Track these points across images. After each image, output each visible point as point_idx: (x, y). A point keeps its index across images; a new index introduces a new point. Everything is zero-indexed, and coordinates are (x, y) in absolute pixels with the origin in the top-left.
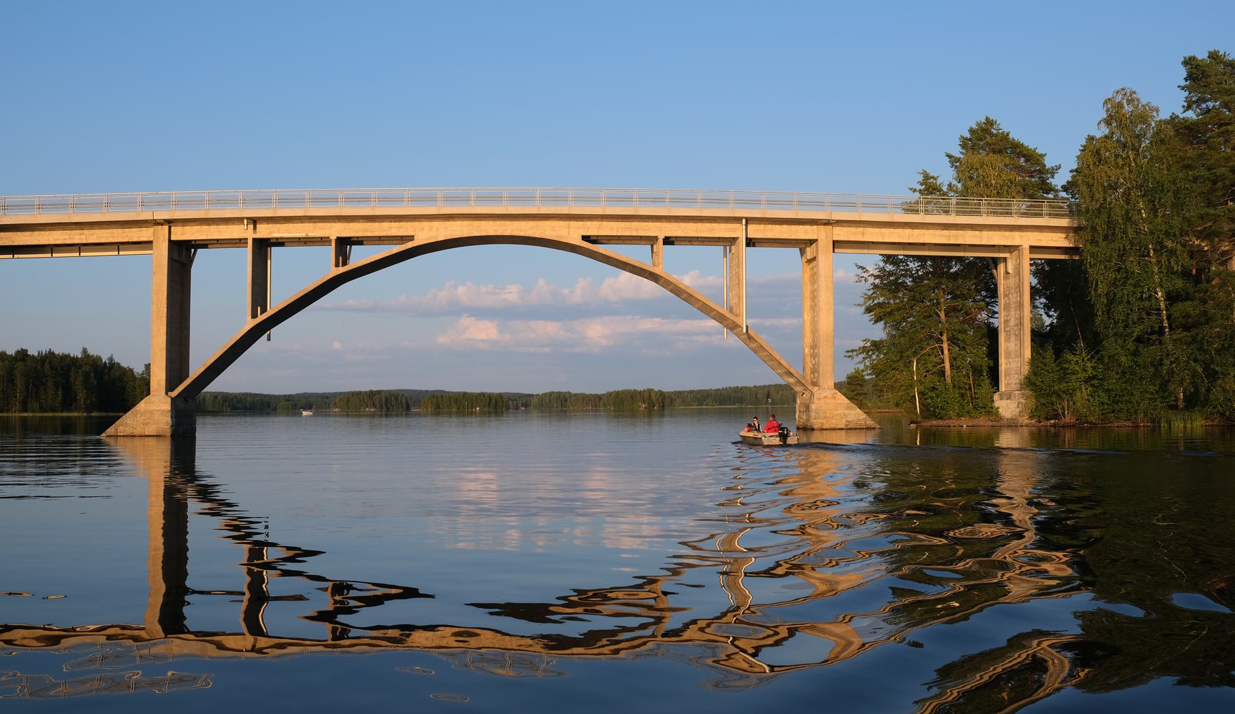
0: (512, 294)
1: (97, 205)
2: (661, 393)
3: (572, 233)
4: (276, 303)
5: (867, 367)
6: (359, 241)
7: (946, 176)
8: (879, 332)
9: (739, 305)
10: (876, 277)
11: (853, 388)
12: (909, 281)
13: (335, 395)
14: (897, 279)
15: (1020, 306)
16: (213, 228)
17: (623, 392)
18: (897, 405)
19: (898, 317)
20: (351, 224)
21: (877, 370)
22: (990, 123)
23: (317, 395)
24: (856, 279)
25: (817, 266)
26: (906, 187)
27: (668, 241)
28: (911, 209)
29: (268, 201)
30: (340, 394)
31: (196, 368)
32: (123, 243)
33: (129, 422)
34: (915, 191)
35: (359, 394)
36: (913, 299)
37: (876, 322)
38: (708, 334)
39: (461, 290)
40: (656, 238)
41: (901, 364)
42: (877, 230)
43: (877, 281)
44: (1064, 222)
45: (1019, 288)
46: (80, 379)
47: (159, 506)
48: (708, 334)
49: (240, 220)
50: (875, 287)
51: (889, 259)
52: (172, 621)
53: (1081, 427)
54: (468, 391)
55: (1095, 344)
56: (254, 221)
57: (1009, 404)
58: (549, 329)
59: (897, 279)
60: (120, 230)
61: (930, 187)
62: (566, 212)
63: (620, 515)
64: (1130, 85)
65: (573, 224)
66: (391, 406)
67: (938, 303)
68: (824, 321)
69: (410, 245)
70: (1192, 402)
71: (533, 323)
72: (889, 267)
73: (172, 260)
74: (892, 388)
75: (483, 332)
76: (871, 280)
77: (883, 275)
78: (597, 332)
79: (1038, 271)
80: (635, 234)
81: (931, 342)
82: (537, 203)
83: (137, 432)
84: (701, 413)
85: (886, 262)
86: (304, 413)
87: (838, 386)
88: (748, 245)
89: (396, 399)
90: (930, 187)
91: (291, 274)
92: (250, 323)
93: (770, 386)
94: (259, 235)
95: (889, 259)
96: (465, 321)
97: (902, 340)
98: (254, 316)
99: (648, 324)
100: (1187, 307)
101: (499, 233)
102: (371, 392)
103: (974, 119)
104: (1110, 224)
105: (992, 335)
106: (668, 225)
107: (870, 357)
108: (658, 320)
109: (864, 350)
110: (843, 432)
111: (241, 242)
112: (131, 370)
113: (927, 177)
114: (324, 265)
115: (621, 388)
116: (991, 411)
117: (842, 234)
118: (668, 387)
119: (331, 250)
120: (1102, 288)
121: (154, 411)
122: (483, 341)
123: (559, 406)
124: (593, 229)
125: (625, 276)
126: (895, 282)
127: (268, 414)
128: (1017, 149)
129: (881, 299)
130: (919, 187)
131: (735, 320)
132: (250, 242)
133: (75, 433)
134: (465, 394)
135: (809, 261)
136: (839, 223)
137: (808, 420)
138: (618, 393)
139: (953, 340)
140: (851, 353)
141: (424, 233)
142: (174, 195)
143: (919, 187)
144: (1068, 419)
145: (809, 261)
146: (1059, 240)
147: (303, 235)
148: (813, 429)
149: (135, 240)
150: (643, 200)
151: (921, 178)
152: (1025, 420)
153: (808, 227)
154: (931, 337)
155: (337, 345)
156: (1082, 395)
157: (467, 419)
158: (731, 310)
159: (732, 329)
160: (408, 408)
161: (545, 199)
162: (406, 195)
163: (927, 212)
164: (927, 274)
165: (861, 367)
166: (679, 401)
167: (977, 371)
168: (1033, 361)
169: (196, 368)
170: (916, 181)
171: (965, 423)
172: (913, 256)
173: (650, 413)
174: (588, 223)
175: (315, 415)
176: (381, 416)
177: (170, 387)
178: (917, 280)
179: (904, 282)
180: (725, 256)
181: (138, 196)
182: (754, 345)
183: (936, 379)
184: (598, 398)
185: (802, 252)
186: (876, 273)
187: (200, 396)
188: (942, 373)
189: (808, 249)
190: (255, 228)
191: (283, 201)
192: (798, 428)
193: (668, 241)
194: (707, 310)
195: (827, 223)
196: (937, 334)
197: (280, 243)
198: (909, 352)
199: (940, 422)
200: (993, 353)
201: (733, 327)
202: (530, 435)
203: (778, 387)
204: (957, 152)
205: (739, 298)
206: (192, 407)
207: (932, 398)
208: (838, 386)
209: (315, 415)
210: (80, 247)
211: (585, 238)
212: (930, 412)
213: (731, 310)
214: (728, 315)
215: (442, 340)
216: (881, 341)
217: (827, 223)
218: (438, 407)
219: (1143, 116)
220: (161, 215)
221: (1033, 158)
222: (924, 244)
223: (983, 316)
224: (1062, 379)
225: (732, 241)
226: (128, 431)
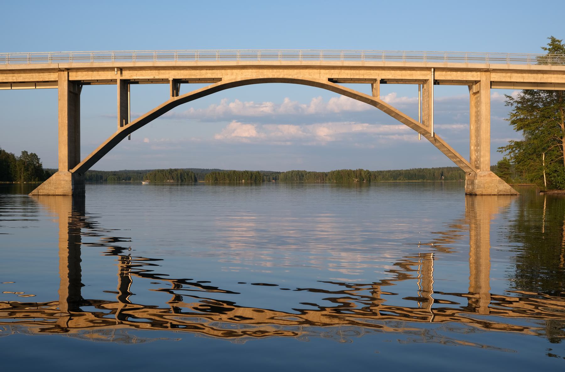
0: (267, 108)
1: (24, 59)
2: (368, 172)
3: (323, 77)
4: (132, 121)
5: (512, 158)
6: (186, 81)
8: (520, 136)
9: (429, 119)
10: (519, 102)
11: (502, 170)
12: (540, 105)
13: (146, 172)
14: (533, 104)
16: (95, 73)
17: (342, 171)
18: (532, 181)
19: (533, 128)
20: (182, 71)
21: (519, 160)
23: (134, 172)
24: (505, 104)
25: (480, 97)
26: (540, 46)
27: (383, 81)
29: (130, 57)
30: (149, 171)
31: (85, 157)
32: (38, 82)
33: (46, 187)
34: (546, 49)
35: (162, 171)
36: (543, 116)
37: (518, 130)
38: (400, 134)
39: (232, 105)
40: (375, 80)
41: (534, 156)
42: (520, 75)
43: (519, 105)
47: (65, 235)
49: (112, 69)
50: (518, 108)
51: (526, 92)
52: (76, 302)
54: (128, 169)
56: (121, 69)
58: (291, 130)
59: (533, 104)
60: (37, 74)
62: (319, 64)
63: (343, 246)
65: (323, 71)
66: (184, 178)
67: (560, 119)
69: (219, 84)
71: (280, 127)
72: (528, 97)
73: (69, 92)
74: (528, 170)
75: (247, 132)
76: (515, 105)
77: (523, 101)
78: (323, 132)
80: (362, 77)
81: (555, 142)
82: (300, 59)
83: (51, 192)
84: (395, 185)
85: (524, 93)
86: (143, 183)
88: (435, 83)
89: (188, 175)
91: (142, 101)
92: (119, 130)
93: (443, 168)
94: (124, 77)
95: (526, 92)
96: (234, 124)
97: (535, 141)
98: (122, 125)
99: (358, 128)
101: (275, 77)
102: (171, 170)
106: (383, 72)
107: (514, 151)
108: (367, 125)
109: (510, 147)
110: (496, 197)
111: (113, 81)
112: (13, 155)
113: (554, 40)
114: (165, 95)
115: (340, 168)
117: (495, 77)
119: (169, 86)
121: (62, 181)
122: (246, 138)
123: (298, 179)
124: (335, 74)
125: (343, 98)
126: (532, 106)
127: (101, 183)
129: (522, 116)
130: (548, 47)
131: (427, 129)
132: (118, 82)
133: (15, 193)
134: (234, 171)
135: (475, 94)
136: (495, 70)
137: (473, 189)
138: (339, 172)
141: (228, 77)
142: (71, 53)
143: (548, 47)
145: (475, 94)
147: (152, 77)
148: (476, 195)
149: (47, 80)
150: (367, 57)
151: (550, 41)
153: (474, 73)
154: (554, 140)
155: (146, 140)
157: (236, 188)
158: (423, 123)
159: (423, 135)
160: (196, 180)
161: (305, 56)
162: (217, 54)
163: (554, 64)
164: (552, 101)
165: (508, 157)
166: (380, 177)
169: (85, 157)
170: (546, 43)
172: (544, 90)
173: (360, 185)
174: (332, 71)
175: (150, 184)
176: (178, 185)
177: (71, 167)
179: (537, 106)
180: (420, 90)
181: (49, 54)
182: (438, 144)
183: (557, 165)
185: (470, 88)
186: (519, 100)
187: (87, 173)
189: (474, 87)
190: (121, 73)
192: (466, 194)
193: (383, 81)
195: (487, 70)
196: (558, 138)
197: (136, 82)
198: (540, 149)
199: (560, 192)
201: (425, 133)
202: (279, 198)
203: (450, 169)
205: (429, 116)
206: (84, 177)
207: (554, 177)
208: (492, 169)
209: (150, 184)
210: (11, 84)
211: (330, 80)
212: (552, 185)
213: (423, 123)
214: (421, 125)
215: (218, 137)
216: (521, 142)
217: (487, 70)
218: (216, 179)
220: (62, 66)
222: (551, 83)
225: (425, 81)
226: (46, 192)
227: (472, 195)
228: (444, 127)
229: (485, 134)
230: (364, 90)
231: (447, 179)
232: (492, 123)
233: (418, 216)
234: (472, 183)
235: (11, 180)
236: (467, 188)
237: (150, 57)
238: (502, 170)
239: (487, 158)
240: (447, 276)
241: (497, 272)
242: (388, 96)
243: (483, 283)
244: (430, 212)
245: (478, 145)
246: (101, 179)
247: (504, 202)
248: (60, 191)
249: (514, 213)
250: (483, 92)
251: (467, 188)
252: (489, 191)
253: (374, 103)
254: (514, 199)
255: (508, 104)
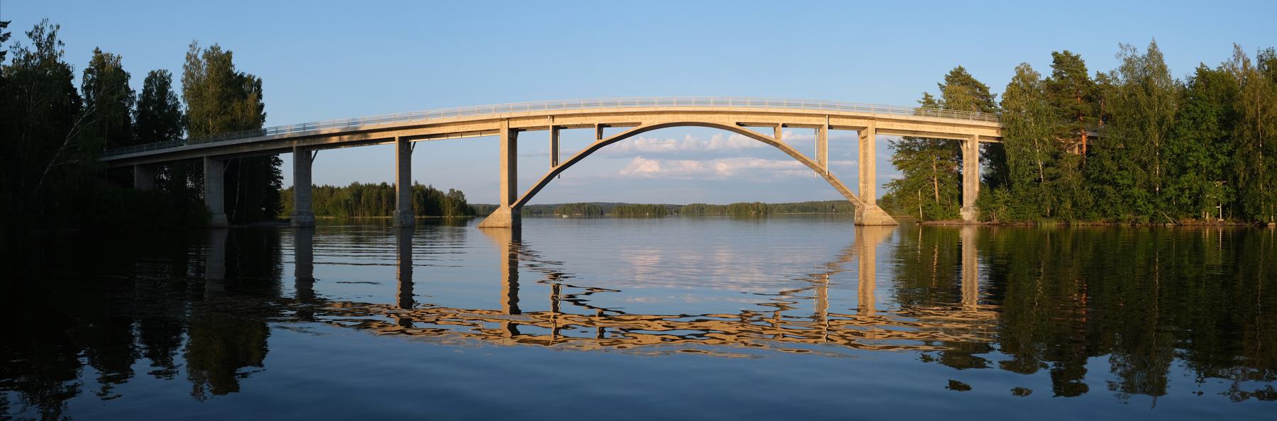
2: (765, 205)
3: (731, 121)
4: (563, 160)
6: (609, 126)
7: (938, 95)
8: (900, 175)
11: (885, 203)
15: (974, 165)
22: (961, 69)
26: (915, 102)
27: (784, 125)
28: (917, 112)
31: (521, 194)
33: (491, 220)
44: (996, 125)
45: (973, 155)
46: (1069, 241)
48: (795, 169)
49: (546, 117)
53: (1002, 225)
55: (1010, 186)
56: (553, 117)
57: (968, 213)
58: (692, 165)
61: (928, 101)
63: (739, 273)
64: (1028, 62)
66: (591, 212)
68: (871, 174)
70: (1052, 214)
74: (908, 204)
77: (902, 145)
78: (722, 167)
79: (986, 146)
84: (790, 217)
87: (878, 202)
90: (928, 101)
91: (572, 143)
92: (552, 170)
96: (638, 160)
99: (755, 163)
100: (1051, 170)
103: (948, 69)
104: (1017, 128)
105: (960, 178)
111: (546, 127)
113: (927, 95)
114: (591, 138)
115: (739, 202)
116: (958, 217)
117: (880, 125)
118: (769, 201)
119: (595, 130)
120: (1012, 159)
121: (504, 215)
123: (699, 212)
124: (742, 119)
128: (975, 84)
139: (940, 181)
140: (885, 186)
141: (647, 121)
144: (996, 221)
146: (993, 133)
152: (975, 221)
156: (1002, 209)
167: (953, 197)
168: (980, 192)
169: (521, 194)
171: (945, 223)
173: (758, 216)
177: (511, 202)
178: (922, 149)
184: (725, 207)
188: (934, 197)
191: (569, 106)
193: (784, 125)
194: (796, 157)
195: (873, 119)
197: (565, 127)
200: (961, 188)
201: (821, 172)
203: (840, 202)
204: (944, 83)
210: (462, 133)
212: (927, 217)
215: (623, 172)
217: (873, 119)
219: (1033, 77)
221: (983, 89)
223: (956, 168)
224: (993, 202)
225: (821, 126)
227: (860, 225)
228: (835, 163)
229: (872, 175)
230: (768, 133)
231: (838, 212)
232: (877, 160)
233: (809, 246)
234: (861, 215)
235: (441, 214)
236: (857, 219)
237: (578, 105)
238: (885, 203)
239: (872, 198)
240: (838, 301)
241: (879, 289)
242: (786, 136)
243: (870, 301)
244: (822, 241)
245: (865, 182)
246: (540, 212)
247: (887, 231)
248: (501, 224)
249: (896, 239)
250: (870, 137)
251: (857, 219)
252: (875, 222)
253: (777, 145)
254: (895, 229)
255: (890, 147)
